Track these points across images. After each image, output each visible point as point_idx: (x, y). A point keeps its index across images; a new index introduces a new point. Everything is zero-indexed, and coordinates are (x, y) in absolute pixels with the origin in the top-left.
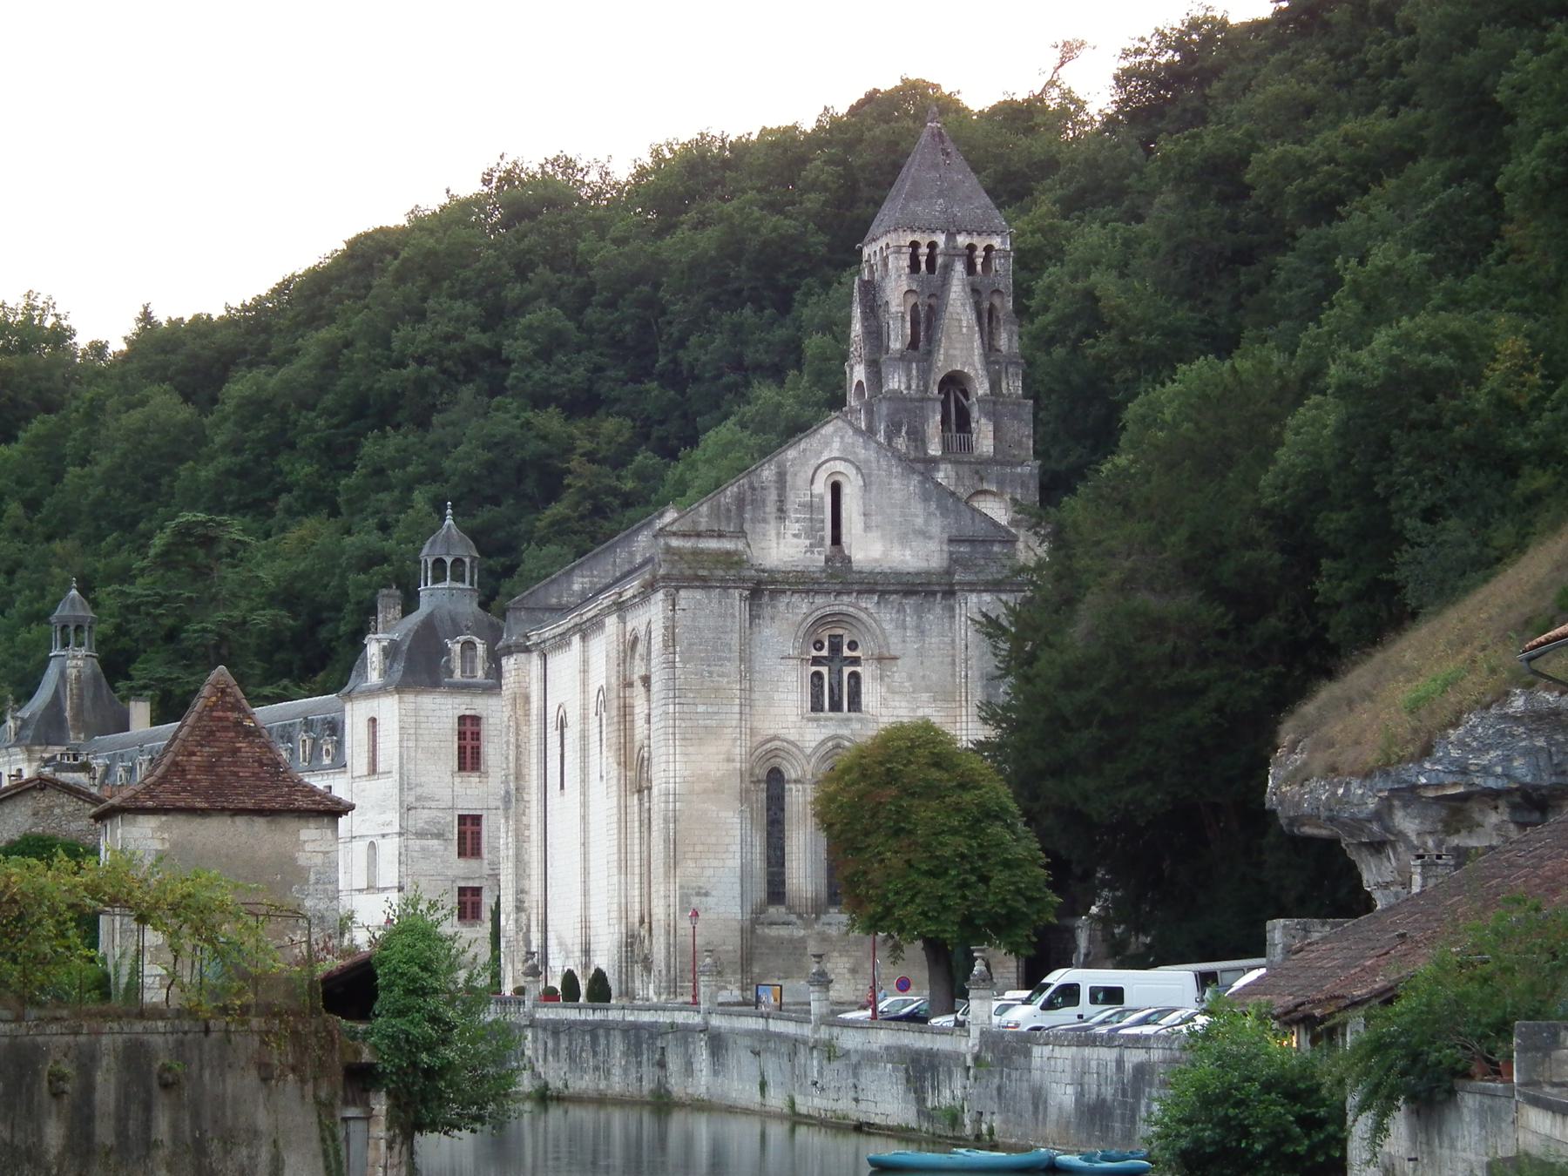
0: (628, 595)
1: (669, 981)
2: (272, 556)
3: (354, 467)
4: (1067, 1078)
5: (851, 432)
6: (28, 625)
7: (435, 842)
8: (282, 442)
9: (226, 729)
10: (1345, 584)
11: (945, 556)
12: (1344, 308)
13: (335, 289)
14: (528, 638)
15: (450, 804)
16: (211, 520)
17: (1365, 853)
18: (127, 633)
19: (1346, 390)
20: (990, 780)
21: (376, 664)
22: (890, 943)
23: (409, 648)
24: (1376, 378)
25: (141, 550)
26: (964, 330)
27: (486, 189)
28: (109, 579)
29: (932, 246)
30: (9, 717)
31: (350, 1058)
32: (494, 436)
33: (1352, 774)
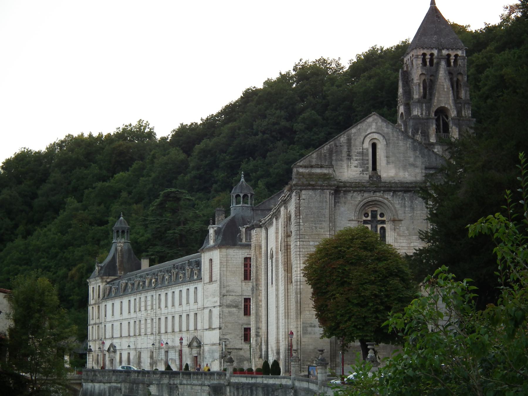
7: (235, 309)
15: (241, 294)
16: (177, 191)
23: (224, 231)
26: (446, 89)
29: (432, 55)
30: (96, 266)
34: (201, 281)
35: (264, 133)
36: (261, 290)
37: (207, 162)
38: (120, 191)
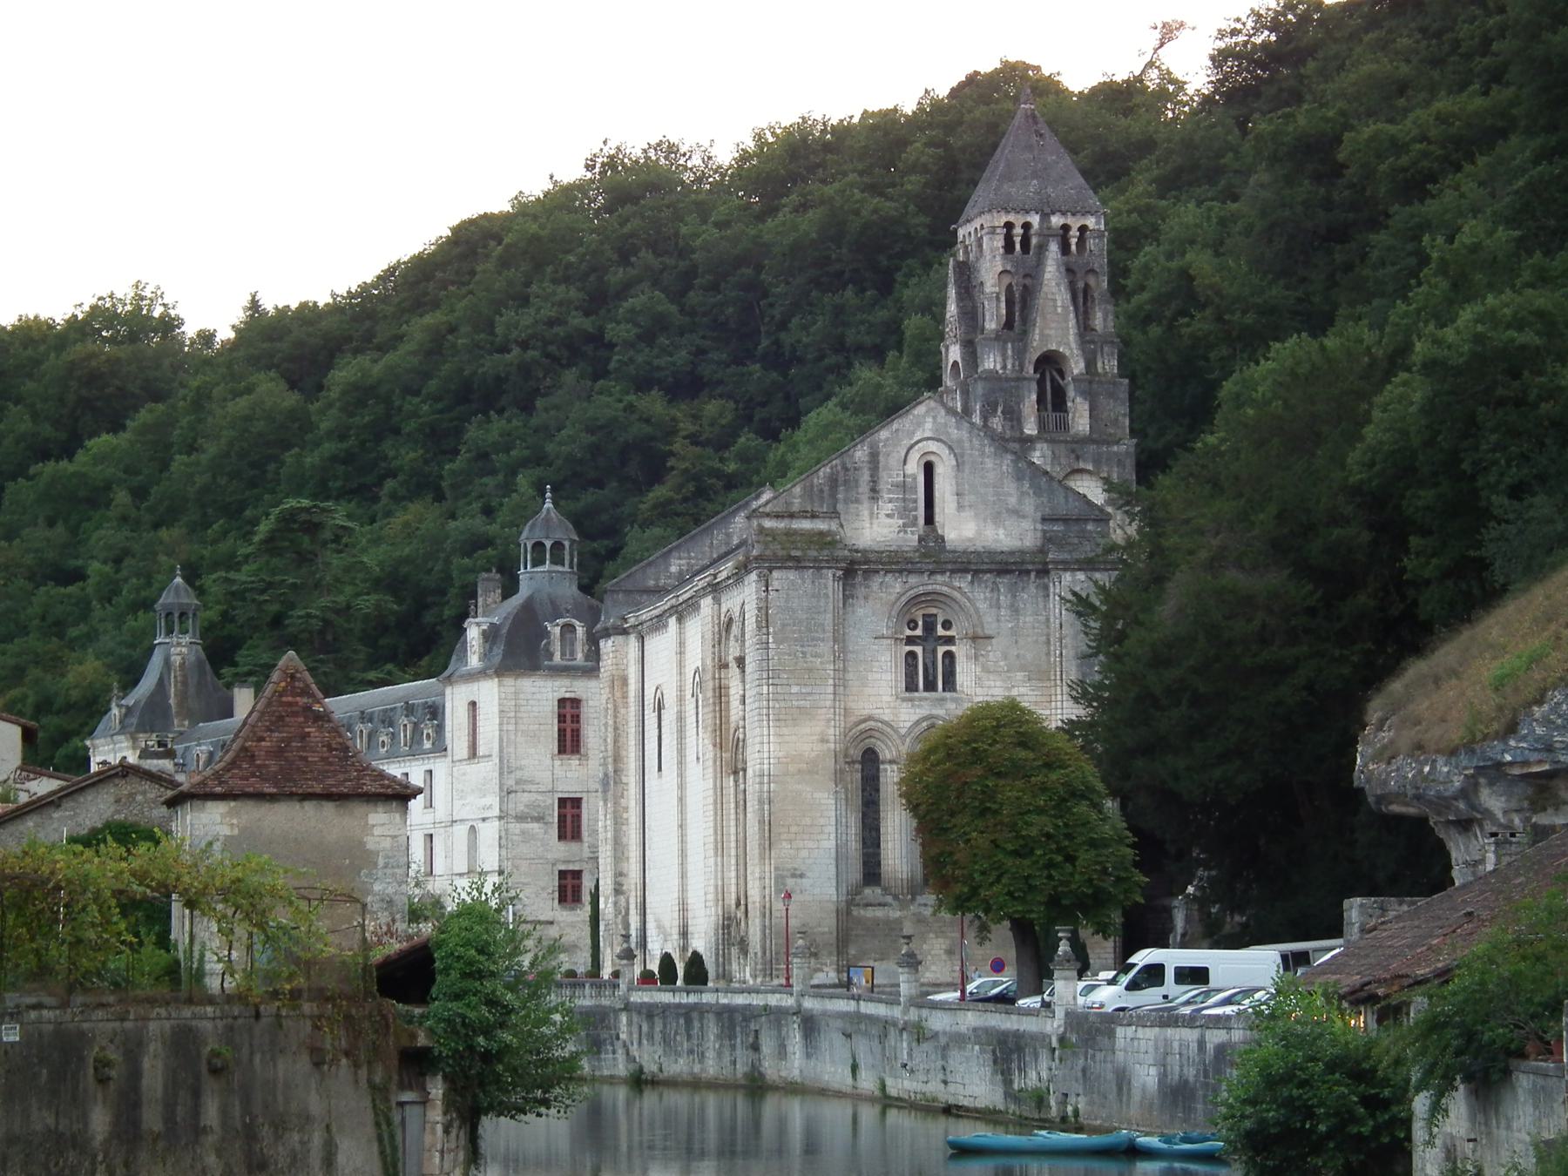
0: (723, 576)
1: (764, 964)
2: (376, 541)
3: (456, 452)
4: (1150, 1058)
5: (943, 412)
6: (135, 612)
7: (535, 825)
8: (386, 428)
9: (295, 714)
10: (1435, 561)
11: (1039, 535)
12: (1432, 287)
13: (439, 275)
14: (626, 620)
15: (550, 787)
16: (315, 506)
17: (1453, 831)
18: (233, 620)
19: (1430, 367)
20: (1077, 759)
21: (476, 648)
22: (977, 923)
23: (509, 631)
24: (1462, 355)
25: (247, 536)
26: (1059, 310)
27: (589, 175)
28: (215, 566)
29: (1027, 226)
30: (113, 704)
31: (405, 1042)
32: (597, 419)
33: (1438, 751)
34: (445, 756)
35: (524, 345)
36: (627, 784)
37: (367, 418)
38: (108, 487)
